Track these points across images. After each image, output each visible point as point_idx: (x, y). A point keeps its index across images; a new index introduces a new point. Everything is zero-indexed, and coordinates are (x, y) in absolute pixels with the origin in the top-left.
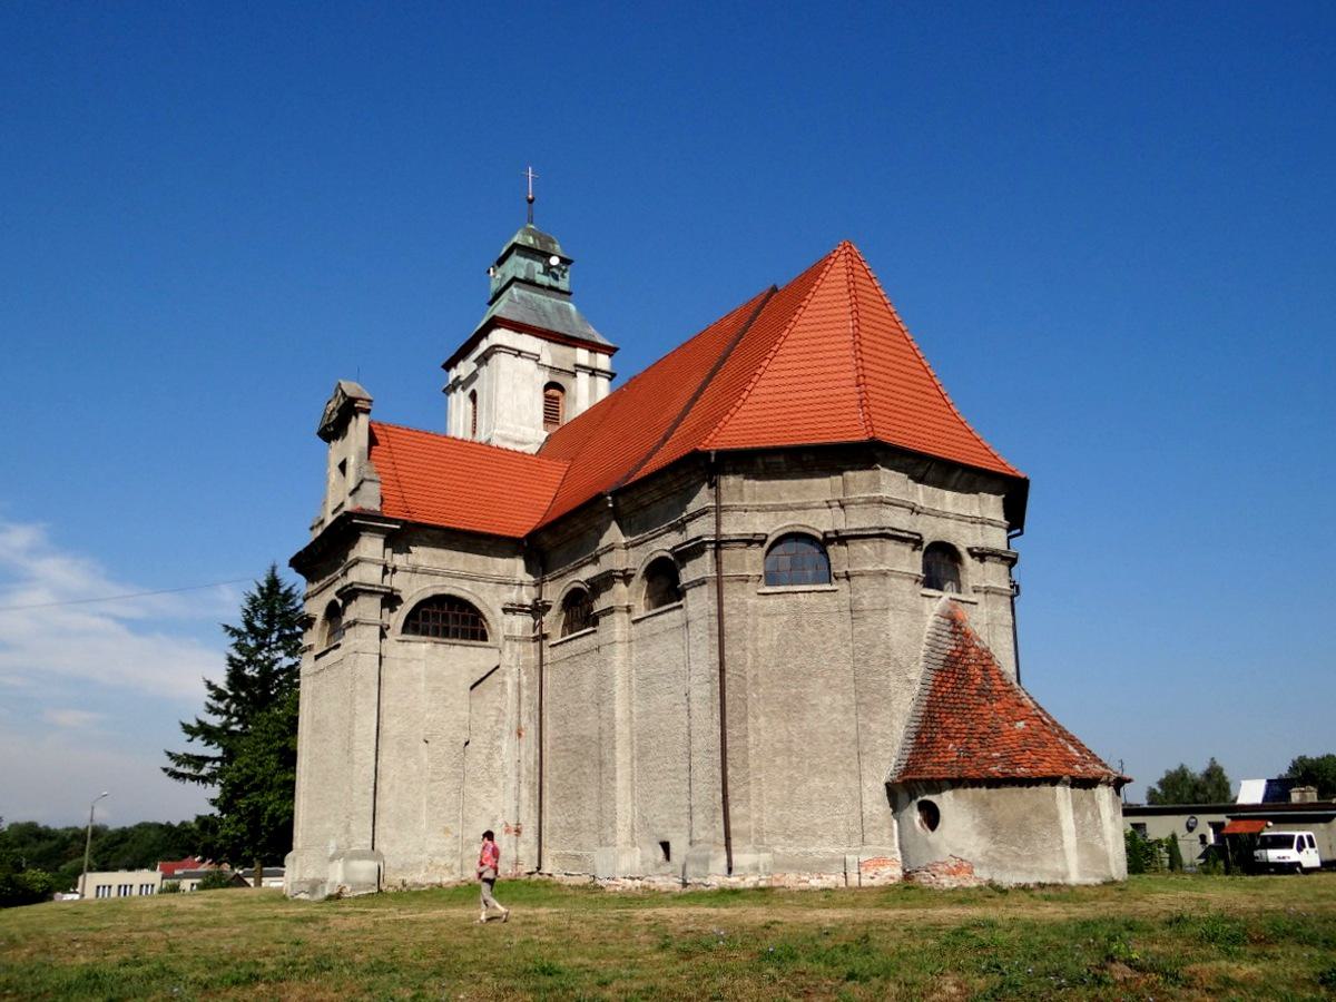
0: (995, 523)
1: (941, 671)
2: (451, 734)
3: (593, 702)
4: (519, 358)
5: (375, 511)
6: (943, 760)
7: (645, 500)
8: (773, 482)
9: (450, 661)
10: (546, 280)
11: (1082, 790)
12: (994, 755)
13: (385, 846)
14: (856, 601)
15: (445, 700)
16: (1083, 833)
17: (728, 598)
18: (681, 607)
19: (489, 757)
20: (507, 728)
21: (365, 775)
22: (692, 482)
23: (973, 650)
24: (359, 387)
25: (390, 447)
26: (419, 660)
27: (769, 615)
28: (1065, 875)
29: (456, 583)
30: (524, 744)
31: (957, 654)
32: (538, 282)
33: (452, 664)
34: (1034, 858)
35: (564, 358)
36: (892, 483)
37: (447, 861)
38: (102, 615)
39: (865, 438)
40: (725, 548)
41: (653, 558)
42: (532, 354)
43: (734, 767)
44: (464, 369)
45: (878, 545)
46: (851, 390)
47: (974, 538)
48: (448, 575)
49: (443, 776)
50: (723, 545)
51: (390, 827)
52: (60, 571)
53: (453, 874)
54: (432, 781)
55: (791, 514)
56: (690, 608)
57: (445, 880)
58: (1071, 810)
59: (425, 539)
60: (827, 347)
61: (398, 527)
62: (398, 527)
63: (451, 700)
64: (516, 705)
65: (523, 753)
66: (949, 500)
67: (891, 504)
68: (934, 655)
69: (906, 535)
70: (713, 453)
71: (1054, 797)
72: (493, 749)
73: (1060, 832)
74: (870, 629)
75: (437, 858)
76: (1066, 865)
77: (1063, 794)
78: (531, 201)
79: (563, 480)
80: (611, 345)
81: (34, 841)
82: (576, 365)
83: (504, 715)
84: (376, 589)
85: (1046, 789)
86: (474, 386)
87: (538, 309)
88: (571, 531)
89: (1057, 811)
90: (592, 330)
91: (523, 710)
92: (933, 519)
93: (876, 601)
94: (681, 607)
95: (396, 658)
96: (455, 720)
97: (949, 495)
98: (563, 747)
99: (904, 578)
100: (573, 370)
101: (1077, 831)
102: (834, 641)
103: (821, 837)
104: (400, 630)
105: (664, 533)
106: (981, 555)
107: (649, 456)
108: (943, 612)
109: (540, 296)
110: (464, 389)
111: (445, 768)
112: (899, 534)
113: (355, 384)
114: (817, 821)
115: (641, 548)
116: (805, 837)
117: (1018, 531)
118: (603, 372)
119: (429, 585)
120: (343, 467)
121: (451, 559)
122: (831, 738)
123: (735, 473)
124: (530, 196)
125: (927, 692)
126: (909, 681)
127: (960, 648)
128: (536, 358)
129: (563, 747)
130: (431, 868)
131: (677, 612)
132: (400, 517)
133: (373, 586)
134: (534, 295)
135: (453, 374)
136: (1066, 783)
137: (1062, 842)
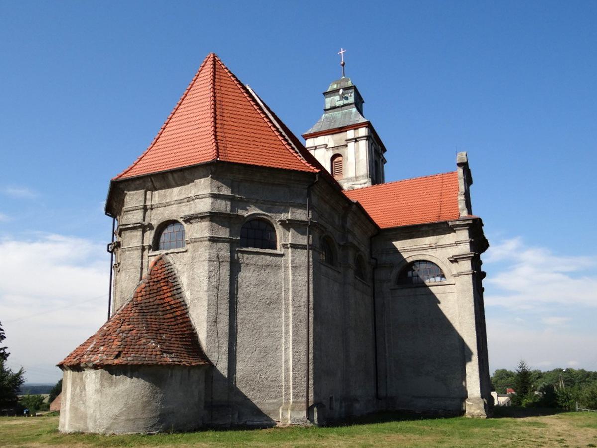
0: (200, 196)
4: (317, 150)
5: (466, 216)
11: (77, 373)
16: (73, 400)
32: (337, 105)
35: (341, 140)
38: (556, 272)
42: (322, 145)
52: (532, 256)
67: (130, 211)
69: (132, 226)
81: (506, 377)
82: (346, 141)
87: (334, 119)
106: (189, 219)
112: (127, 227)
118: (361, 137)
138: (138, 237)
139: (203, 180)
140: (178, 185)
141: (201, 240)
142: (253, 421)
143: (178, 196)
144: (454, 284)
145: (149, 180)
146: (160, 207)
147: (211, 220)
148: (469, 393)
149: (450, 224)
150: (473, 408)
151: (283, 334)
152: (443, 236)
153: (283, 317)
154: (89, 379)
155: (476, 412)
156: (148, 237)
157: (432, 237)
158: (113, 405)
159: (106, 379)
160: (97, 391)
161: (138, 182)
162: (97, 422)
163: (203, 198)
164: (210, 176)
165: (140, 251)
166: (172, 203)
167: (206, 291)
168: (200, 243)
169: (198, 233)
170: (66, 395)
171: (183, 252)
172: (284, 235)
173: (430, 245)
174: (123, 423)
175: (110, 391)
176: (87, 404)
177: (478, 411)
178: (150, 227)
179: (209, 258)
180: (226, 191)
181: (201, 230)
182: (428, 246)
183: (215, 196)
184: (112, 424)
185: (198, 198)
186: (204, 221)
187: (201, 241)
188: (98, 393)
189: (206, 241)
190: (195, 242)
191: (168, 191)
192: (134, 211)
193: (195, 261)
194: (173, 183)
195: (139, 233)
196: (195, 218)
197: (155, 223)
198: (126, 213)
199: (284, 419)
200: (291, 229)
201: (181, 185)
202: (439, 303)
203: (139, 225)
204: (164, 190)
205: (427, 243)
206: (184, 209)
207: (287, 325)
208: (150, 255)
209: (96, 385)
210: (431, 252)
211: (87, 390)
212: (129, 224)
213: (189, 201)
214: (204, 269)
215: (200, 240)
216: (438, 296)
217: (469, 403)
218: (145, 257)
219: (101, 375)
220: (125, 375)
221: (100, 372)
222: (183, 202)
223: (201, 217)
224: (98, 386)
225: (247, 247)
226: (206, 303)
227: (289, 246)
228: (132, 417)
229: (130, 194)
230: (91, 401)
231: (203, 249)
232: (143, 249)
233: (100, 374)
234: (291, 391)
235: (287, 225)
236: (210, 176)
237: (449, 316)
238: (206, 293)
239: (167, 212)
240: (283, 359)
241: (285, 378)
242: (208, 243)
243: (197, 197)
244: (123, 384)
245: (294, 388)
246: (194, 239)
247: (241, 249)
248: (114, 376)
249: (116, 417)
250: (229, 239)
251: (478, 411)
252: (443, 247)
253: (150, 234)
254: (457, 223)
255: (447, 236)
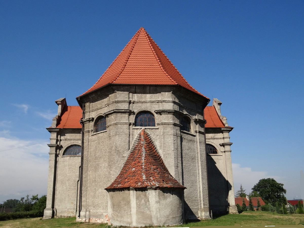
0: (167, 101)
2: (74, 179)
8: (96, 102)
9: (74, 161)
11: (141, 192)
13: (57, 207)
15: (73, 170)
21: (50, 190)
25: (208, 109)
26: (67, 161)
27: (93, 141)
28: (131, 223)
29: (77, 141)
33: (75, 161)
34: (122, 217)
36: (121, 96)
37: (72, 210)
40: (85, 124)
43: (84, 186)
45: (115, 115)
47: (159, 107)
48: (74, 140)
49: (71, 189)
50: (84, 123)
51: (59, 202)
53: (74, 214)
54: (69, 191)
57: (71, 215)
58: (135, 199)
59: (68, 132)
61: (58, 130)
62: (58, 130)
63: (74, 170)
66: (148, 97)
67: (120, 102)
71: (129, 194)
73: (130, 208)
75: (69, 210)
76: (131, 219)
77: (132, 194)
84: (53, 145)
85: (126, 192)
89: (130, 200)
92: (140, 104)
95: (61, 161)
97: (148, 96)
99: (124, 124)
101: (137, 207)
102: (106, 146)
103: (100, 207)
104: (62, 154)
106: (160, 112)
111: (72, 187)
112: (120, 111)
114: (100, 202)
116: (97, 207)
119: (69, 143)
121: (76, 136)
122: (104, 176)
123: (88, 102)
126: (123, 157)
130: (68, 212)
133: (52, 145)
136: (132, 190)
137: (131, 211)
138: (126, 117)
139: (167, 93)
140: (150, 93)
141: (168, 124)
142: (191, 218)
143: (150, 99)
144: (222, 156)
145: (135, 87)
146: (139, 103)
147: (173, 115)
148: (230, 204)
149: (222, 129)
150: (233, 210)
151: (198, 175)
152: (217, 134)
153: (197, 166)
154: (151, 196)
155: (234, 212)
156: (132, 118)
157: (212, 134)
158: (166, 210)
159: (161, 195)
160: (157, 202)
161: (127, 87)
162: (159, 220)
163: (168, 102)
164: (172, 92)
165: (128, 125)
166: (148, 102)
167: (173, 151)
168: (167, 125)
169: (166, 120)
170: (130, 205)
171: (156, 129)
172: (195, 126)
173: (211, 137)
174: (171, 220)
175: (163, 202)
176: (151, 210)
177: (235, 211)
178: (134, 113)
179: (174, 134)
180: (177, 101)
181: (169, 119)
182: (211, 138)
183: (174, 102)
184: (166, 220)
185: (165, 102)
186: (169, 114)
187: (169, 124)
188: (157, 203)
189: (171, 125)
190: (164, 124)
191: (144, 95)
192: (122, 103)
193: (165, 134)
194: (148, 92)
195: (127, 115)
196: (165, 112)
197: (136, 111)
198: (117, 103)
199: (201, 216)
200: (198, 124)
201: (152, 93)
202: (216, 163)
203: (128, 111)
204: (140, 94)
205: (210, 136)
206: (155, 106)
207: (199, 170)
208: (134, 128)
209: (156, 199)
210: (211, 141)
211: (150, 201)
212: (122, 110)
213: (158, 103)
214: (171, 139)
215: (168, 124)
216: (215, 160)
217: (231, 208)
218: (131, 131)
219: (159, 193)
220: (170, 193)
221: (158, 191)
222: (154, 103)
223: (168, 112)
224: (157, 199)
225: (184, 130)
226: (173, 157)
227: (198, 132)
228: (174, 216)
229: (119, 93)
230: (154, 208)
231: (169, 129)
232: (130, 124)
233: (158, 192)
234: (202, 202)
235: (196, 122)
236: (172, 92)
237: (220, 170)
238: (172, 151)
239: (144, 106)
240: (198, 186)
241: (200, 195)
242: (172, 126)
243: (165, 101)
244: (169, 198)
245: (203, 201)
246: (165, 123)
247: (183, 131)
248: (165, 193)
249: (168, 216)
250: (179, 124)
251: (235, 211)
252: (217, 139)
253: (133, 116)
254: (225, 129)
255: (218, 134)
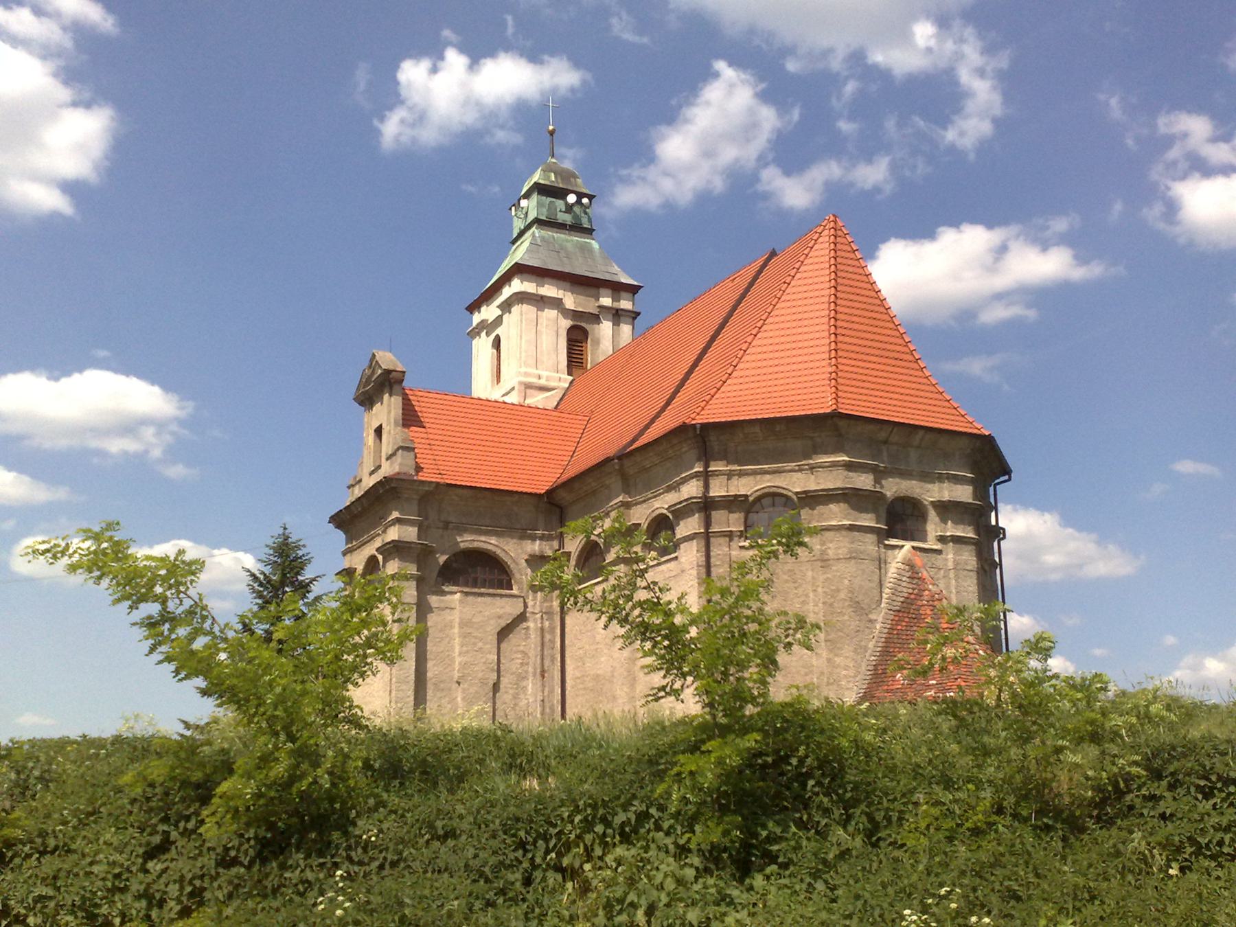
1: (899, 611)
2: (480, 675)
3: (606, 644)
6: (891, 687)
7: (647, 464)
10: (566, 218)
12: (931, 682)
14: (824, 551)
15: (475, 644)
17: (715, 552)
18: (676, 558)
19: (515, 697)
20: (531, 669)
22: (684, 450)
23: (927, 592)
24: (393, 357)
30: (547, 684)
31: (913, 596)
39: (829, 411)
41: (654, 515)
44: (489, 312)
46: (825, 363)
55: (768, 477)
56: (683, 559)
60: (806, 323)
63: (480, 644)
64: (539, 649)
65: (546, 694)
68: (895, 598)
70: (698, 426)
72: (519, 689)
74: (835, 576)
78: (552, 133)
79: (572, 457)
80: (636, 283)
83: (529, 658)
86: (498, 331)
87: (558, 250)
88: (585, 488)
90: (616, 268)
91: (545, 653)
93: (840, 551)
94: (676, 558)
96: (484, 663)
98: (581, 686)
100: (595, 311)
105: (663, 493)
107: (647, 427)
108: (904, 559)
109: (563, 236)
110: (488, 335)
113: (389, 355)
115: (644, 505)
117: (1006, 477)
120: (379, 431)
124: (551, 128)
125: (886, 631)
127: (916, 591)
128: (556, 303)
129: (581, 686)
131: (673, 564)
132: (434, 480)
134: (556, 235)
135: (477, 318)
